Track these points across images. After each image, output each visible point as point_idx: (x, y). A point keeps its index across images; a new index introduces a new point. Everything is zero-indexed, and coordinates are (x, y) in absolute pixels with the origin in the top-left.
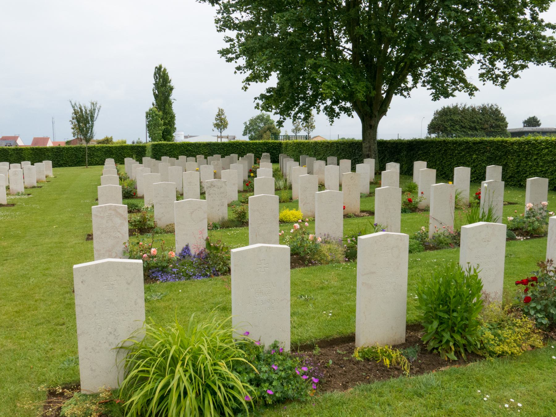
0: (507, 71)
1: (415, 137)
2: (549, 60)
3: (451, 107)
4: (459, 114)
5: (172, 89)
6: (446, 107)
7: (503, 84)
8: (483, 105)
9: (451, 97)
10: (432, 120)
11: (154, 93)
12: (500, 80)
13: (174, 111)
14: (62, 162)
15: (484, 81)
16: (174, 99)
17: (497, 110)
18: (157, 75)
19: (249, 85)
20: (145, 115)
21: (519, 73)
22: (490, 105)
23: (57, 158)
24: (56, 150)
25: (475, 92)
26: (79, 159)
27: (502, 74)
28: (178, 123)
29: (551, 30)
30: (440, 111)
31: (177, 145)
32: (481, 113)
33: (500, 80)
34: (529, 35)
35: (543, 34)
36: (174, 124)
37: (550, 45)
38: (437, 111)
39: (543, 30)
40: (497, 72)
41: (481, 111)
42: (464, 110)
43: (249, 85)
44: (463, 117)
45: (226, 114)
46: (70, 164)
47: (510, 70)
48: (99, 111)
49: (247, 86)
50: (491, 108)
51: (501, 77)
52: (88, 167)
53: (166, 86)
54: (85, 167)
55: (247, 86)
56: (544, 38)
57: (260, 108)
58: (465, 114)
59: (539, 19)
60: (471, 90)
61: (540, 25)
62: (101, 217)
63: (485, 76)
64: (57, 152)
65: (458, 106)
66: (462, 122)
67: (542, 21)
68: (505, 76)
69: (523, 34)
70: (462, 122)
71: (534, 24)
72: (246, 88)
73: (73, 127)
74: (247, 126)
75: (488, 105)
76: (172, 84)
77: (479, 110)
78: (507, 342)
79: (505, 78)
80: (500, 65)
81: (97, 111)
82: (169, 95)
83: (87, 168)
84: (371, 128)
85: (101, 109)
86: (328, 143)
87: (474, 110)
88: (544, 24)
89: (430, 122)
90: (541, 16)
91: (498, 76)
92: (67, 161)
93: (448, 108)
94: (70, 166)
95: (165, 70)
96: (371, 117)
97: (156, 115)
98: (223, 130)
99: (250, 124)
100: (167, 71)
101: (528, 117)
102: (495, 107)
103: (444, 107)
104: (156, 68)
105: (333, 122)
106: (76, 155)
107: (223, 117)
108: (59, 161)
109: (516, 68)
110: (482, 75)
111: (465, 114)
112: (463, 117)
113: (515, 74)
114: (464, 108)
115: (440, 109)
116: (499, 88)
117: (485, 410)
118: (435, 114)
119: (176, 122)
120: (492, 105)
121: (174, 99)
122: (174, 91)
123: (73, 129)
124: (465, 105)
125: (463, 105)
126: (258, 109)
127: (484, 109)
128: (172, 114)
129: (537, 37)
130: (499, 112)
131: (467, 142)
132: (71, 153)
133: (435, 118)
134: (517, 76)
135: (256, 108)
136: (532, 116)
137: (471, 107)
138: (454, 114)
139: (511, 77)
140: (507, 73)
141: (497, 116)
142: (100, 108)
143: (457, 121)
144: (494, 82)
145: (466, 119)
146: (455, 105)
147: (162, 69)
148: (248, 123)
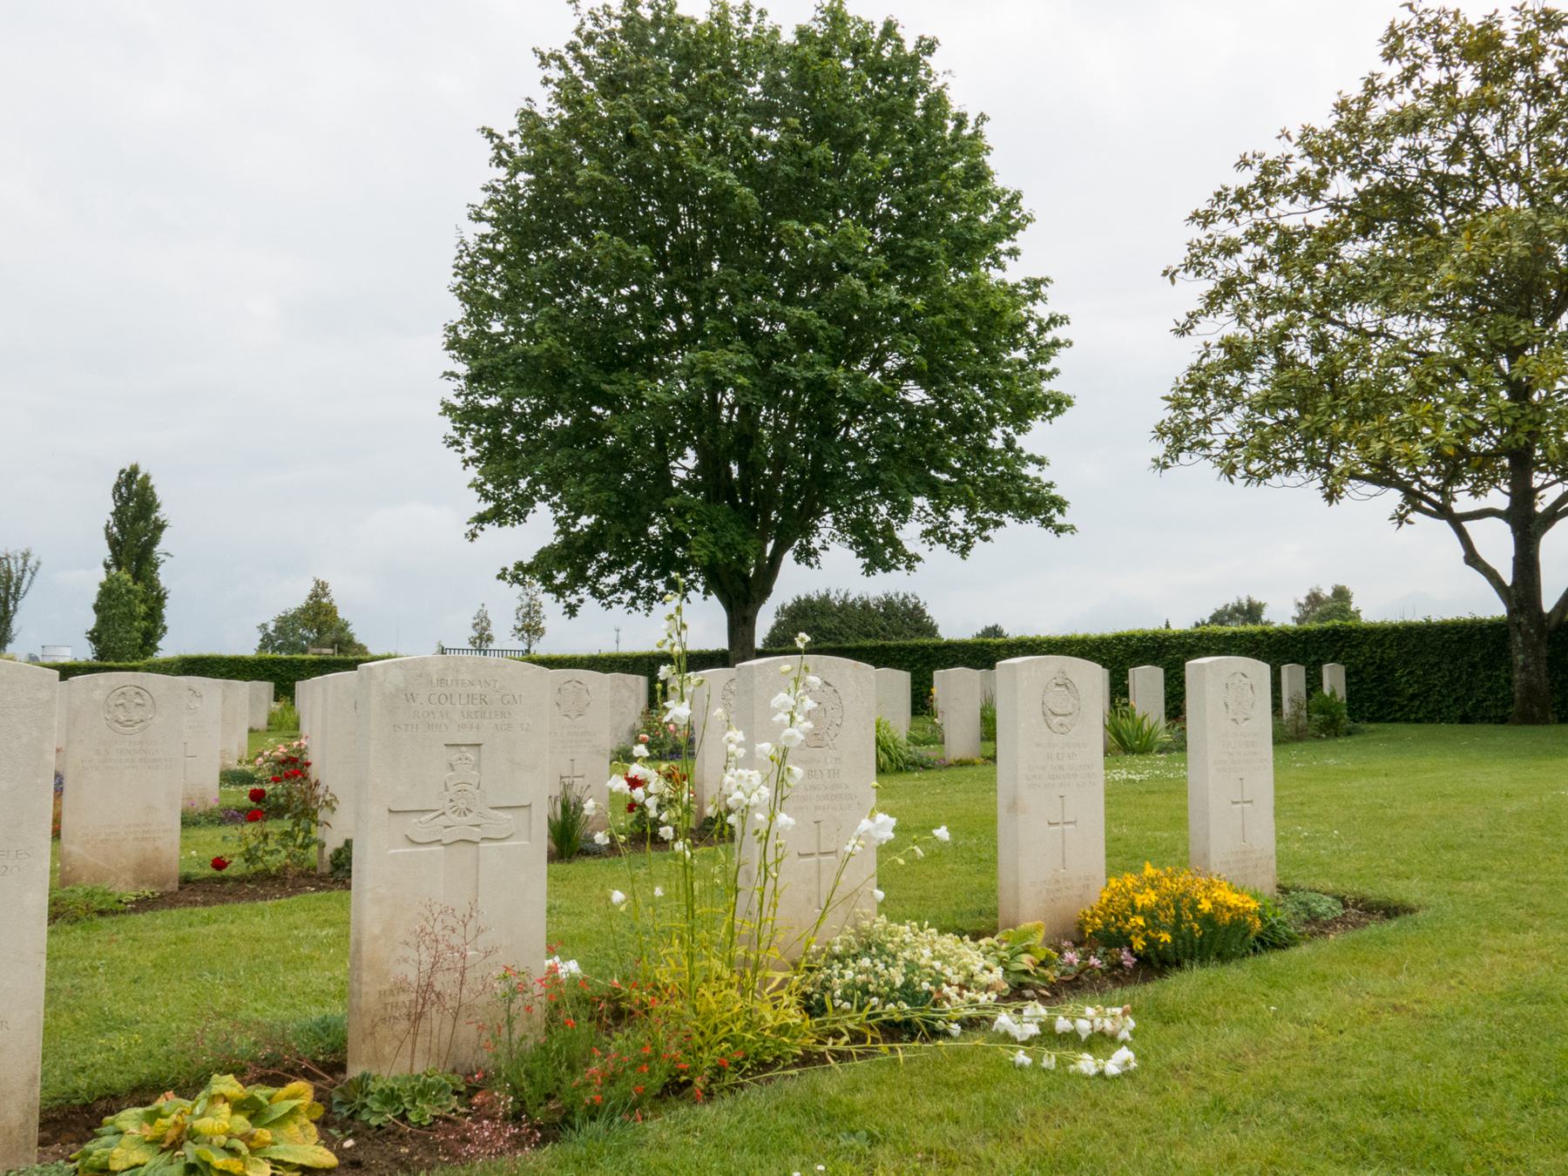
0: (971, 528)
2: (1036, 514)
3: (815, 599)
4: (833, 614)
5: (160, 527)
6: (803, 597)
7: (964, 551)
8: (886, 596)
9: (893, 571)
10: (773, 629)
11: (109, 536)
12: (959, 543)
15: (931, 544)
16: (167, 554)
17: (916, 607)
18: (123, 490)
19: (482, 529)
21: (989, 532)
22: (901, 596)
25: (916, 564)
27: (961, 533)
28: (171, 613)
29: (1036, 467)
30: (789, 608)
31: (246, 662)
32: (882, 614)
33: (959, 543)
34: (1002, 474)
35: (1024, 471)
36: (161, 617)
37: (1037, 492)
38: (783, 608)
39: (1024, 465)
40: (954, 530)
41: (882, 610)
42: (846, 607)
43: (482, 529)
44: (842, 621)
45: (333, 595)
47: (975, 527)
48: (33, 574)
49: (478, 532)
50: (904, 604)
51: (961, 539)
53: (147, 519)
55: (478, 532)
56: (1026, 479)
57: (509, 578)
58: (847, 615)
59: (1017, 446)
60: (910, 561)
61: (1019, 457)
63: (936, 534)
65: (831, 597)
66: (841, 634)
67: (1021, 451)
68: (967, 537)
69: (993, 470)
70: (841, 634)
71: (1010, 454)
72: (474, 535)
74: (267, 636)
75: (897, 595)
76: (162, 514)
77: (878, 607)
78: (1200, 217)
79: (968, 541)
80: (957, 515)
81: (28, 574)
82: (154, 541)
84: (745, 623)
85: (41, 568)
86: (626, 657)
87: (866, 605)
88: (1024, 455)
89: (768, 631)
90: (1021, 441)
91: (954, 537)
93: (808, 600)
95: (147, 478)
96: (746, 602)
97: (129, 591)
98: (628, 596)
99: (277, 629)
100: (152, 482)
101: (983, 627)
102: (913, 600)
103: (799, 598)
104: (122, 472)
105: (650, 609)
107: (325, 600)
109: (984, 525)
110: (926, 534)
111: (847, 615)
112: (842, 621)
113: (984, 534)
114: (844, 602)
115: (789, 603)
116: (958, 556)
118: (778, 613)
120: (906, 597)
121: (167, 554)
122: (165, 536)
124: (846, 595)
125: (842, 595)
126: (504, 579)
127: (889, 604)
128: (159, 592)
129: (1015, 477)
130: (923, 612)
131: (924, 647)
133: (779, 624)
134: (986, 539)
135: (499, 577)
136: (990, 625)
137: (861, 599)
138: (823, 613)
139: (977, 539)
140: (970, 531)
141: (919, 621)
142: (37, 569)
143: (830, 631)
144: (949, 546)
145: (850, 628)
146: (823, 592)
147: (139, 477)
148: (271, 627)
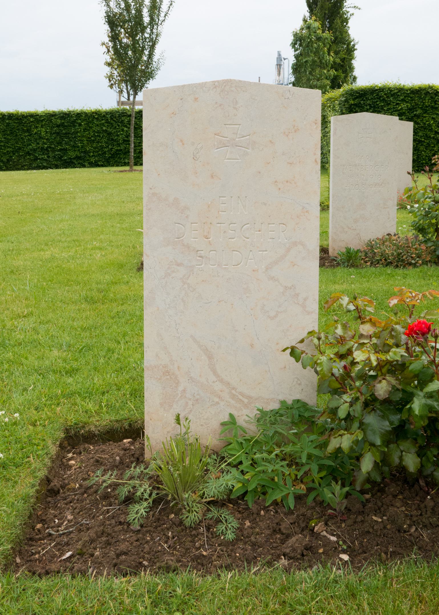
1: (59, 109)
13: (350, 32)
14: (72, 154)
20: (291, 39)
23: (60, 143)
24: (59, 121)
26: (119, 145)
36: (352, 69)
46: (93, 160)
52: (135, 168)
54: (127, 168)
62: (84, 272)
64: (62, 125)
73: (109, 60)
83: (131, 170)
92: (85, 152)
94: (96, 165)
97: (319, 39)
106: (110, 134)
108: (66, 150)
117: (263, 420)
119: (355, 63)
123: (109, 64)
132: (98, 129)
